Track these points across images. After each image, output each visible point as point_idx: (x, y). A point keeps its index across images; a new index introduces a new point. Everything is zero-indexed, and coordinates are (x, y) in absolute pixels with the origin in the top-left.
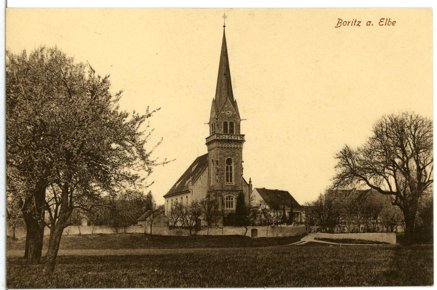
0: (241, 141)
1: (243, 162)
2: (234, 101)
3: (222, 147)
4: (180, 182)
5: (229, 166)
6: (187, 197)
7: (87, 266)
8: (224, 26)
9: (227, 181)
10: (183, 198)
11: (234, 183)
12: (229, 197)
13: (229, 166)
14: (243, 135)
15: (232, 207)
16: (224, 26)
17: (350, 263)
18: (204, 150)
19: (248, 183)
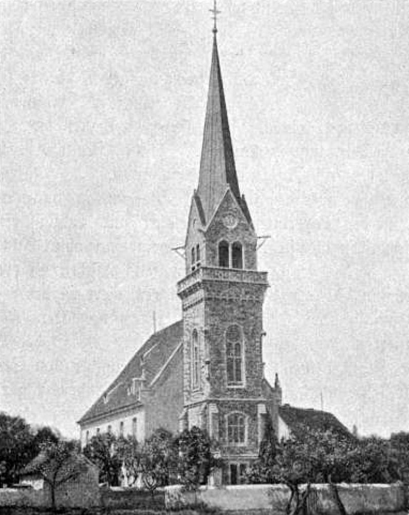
0: (260, 285)
1: (265, 334)
2: (241, 196)
3: (218, 299)
4: (112, 390)
5: (234, 344)
6: (135, 420)
7: (213, 333)
8: (215, 31)
9: (231, 378)
10: (125, 424)
11: (244, 383)
12: (236, 416)
13: (234, 344)
14: (265, 273)
15: (242, 440)
16: (215, 31)
17: (86, 455)
18: (171, 313)
19: (273, 386)
